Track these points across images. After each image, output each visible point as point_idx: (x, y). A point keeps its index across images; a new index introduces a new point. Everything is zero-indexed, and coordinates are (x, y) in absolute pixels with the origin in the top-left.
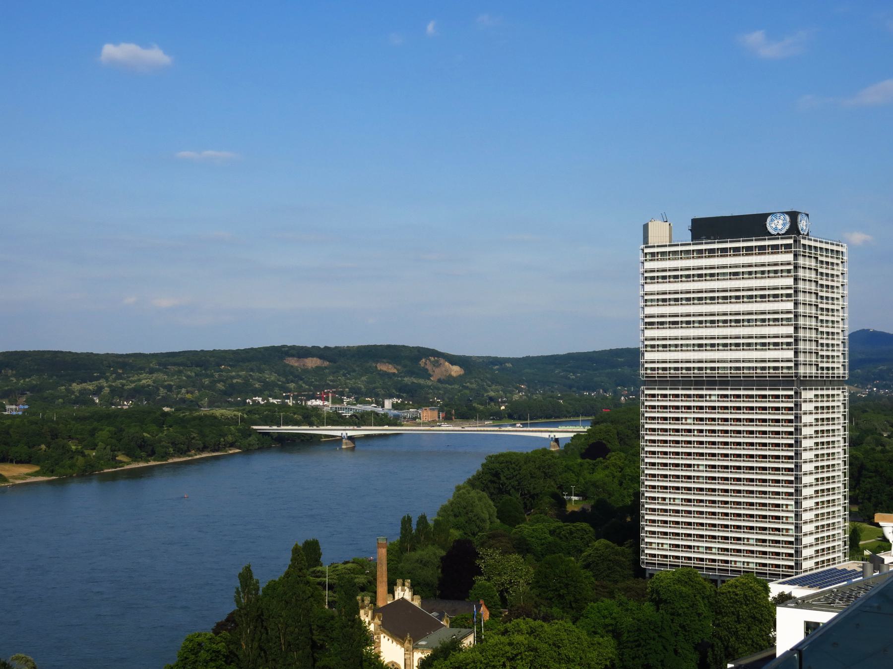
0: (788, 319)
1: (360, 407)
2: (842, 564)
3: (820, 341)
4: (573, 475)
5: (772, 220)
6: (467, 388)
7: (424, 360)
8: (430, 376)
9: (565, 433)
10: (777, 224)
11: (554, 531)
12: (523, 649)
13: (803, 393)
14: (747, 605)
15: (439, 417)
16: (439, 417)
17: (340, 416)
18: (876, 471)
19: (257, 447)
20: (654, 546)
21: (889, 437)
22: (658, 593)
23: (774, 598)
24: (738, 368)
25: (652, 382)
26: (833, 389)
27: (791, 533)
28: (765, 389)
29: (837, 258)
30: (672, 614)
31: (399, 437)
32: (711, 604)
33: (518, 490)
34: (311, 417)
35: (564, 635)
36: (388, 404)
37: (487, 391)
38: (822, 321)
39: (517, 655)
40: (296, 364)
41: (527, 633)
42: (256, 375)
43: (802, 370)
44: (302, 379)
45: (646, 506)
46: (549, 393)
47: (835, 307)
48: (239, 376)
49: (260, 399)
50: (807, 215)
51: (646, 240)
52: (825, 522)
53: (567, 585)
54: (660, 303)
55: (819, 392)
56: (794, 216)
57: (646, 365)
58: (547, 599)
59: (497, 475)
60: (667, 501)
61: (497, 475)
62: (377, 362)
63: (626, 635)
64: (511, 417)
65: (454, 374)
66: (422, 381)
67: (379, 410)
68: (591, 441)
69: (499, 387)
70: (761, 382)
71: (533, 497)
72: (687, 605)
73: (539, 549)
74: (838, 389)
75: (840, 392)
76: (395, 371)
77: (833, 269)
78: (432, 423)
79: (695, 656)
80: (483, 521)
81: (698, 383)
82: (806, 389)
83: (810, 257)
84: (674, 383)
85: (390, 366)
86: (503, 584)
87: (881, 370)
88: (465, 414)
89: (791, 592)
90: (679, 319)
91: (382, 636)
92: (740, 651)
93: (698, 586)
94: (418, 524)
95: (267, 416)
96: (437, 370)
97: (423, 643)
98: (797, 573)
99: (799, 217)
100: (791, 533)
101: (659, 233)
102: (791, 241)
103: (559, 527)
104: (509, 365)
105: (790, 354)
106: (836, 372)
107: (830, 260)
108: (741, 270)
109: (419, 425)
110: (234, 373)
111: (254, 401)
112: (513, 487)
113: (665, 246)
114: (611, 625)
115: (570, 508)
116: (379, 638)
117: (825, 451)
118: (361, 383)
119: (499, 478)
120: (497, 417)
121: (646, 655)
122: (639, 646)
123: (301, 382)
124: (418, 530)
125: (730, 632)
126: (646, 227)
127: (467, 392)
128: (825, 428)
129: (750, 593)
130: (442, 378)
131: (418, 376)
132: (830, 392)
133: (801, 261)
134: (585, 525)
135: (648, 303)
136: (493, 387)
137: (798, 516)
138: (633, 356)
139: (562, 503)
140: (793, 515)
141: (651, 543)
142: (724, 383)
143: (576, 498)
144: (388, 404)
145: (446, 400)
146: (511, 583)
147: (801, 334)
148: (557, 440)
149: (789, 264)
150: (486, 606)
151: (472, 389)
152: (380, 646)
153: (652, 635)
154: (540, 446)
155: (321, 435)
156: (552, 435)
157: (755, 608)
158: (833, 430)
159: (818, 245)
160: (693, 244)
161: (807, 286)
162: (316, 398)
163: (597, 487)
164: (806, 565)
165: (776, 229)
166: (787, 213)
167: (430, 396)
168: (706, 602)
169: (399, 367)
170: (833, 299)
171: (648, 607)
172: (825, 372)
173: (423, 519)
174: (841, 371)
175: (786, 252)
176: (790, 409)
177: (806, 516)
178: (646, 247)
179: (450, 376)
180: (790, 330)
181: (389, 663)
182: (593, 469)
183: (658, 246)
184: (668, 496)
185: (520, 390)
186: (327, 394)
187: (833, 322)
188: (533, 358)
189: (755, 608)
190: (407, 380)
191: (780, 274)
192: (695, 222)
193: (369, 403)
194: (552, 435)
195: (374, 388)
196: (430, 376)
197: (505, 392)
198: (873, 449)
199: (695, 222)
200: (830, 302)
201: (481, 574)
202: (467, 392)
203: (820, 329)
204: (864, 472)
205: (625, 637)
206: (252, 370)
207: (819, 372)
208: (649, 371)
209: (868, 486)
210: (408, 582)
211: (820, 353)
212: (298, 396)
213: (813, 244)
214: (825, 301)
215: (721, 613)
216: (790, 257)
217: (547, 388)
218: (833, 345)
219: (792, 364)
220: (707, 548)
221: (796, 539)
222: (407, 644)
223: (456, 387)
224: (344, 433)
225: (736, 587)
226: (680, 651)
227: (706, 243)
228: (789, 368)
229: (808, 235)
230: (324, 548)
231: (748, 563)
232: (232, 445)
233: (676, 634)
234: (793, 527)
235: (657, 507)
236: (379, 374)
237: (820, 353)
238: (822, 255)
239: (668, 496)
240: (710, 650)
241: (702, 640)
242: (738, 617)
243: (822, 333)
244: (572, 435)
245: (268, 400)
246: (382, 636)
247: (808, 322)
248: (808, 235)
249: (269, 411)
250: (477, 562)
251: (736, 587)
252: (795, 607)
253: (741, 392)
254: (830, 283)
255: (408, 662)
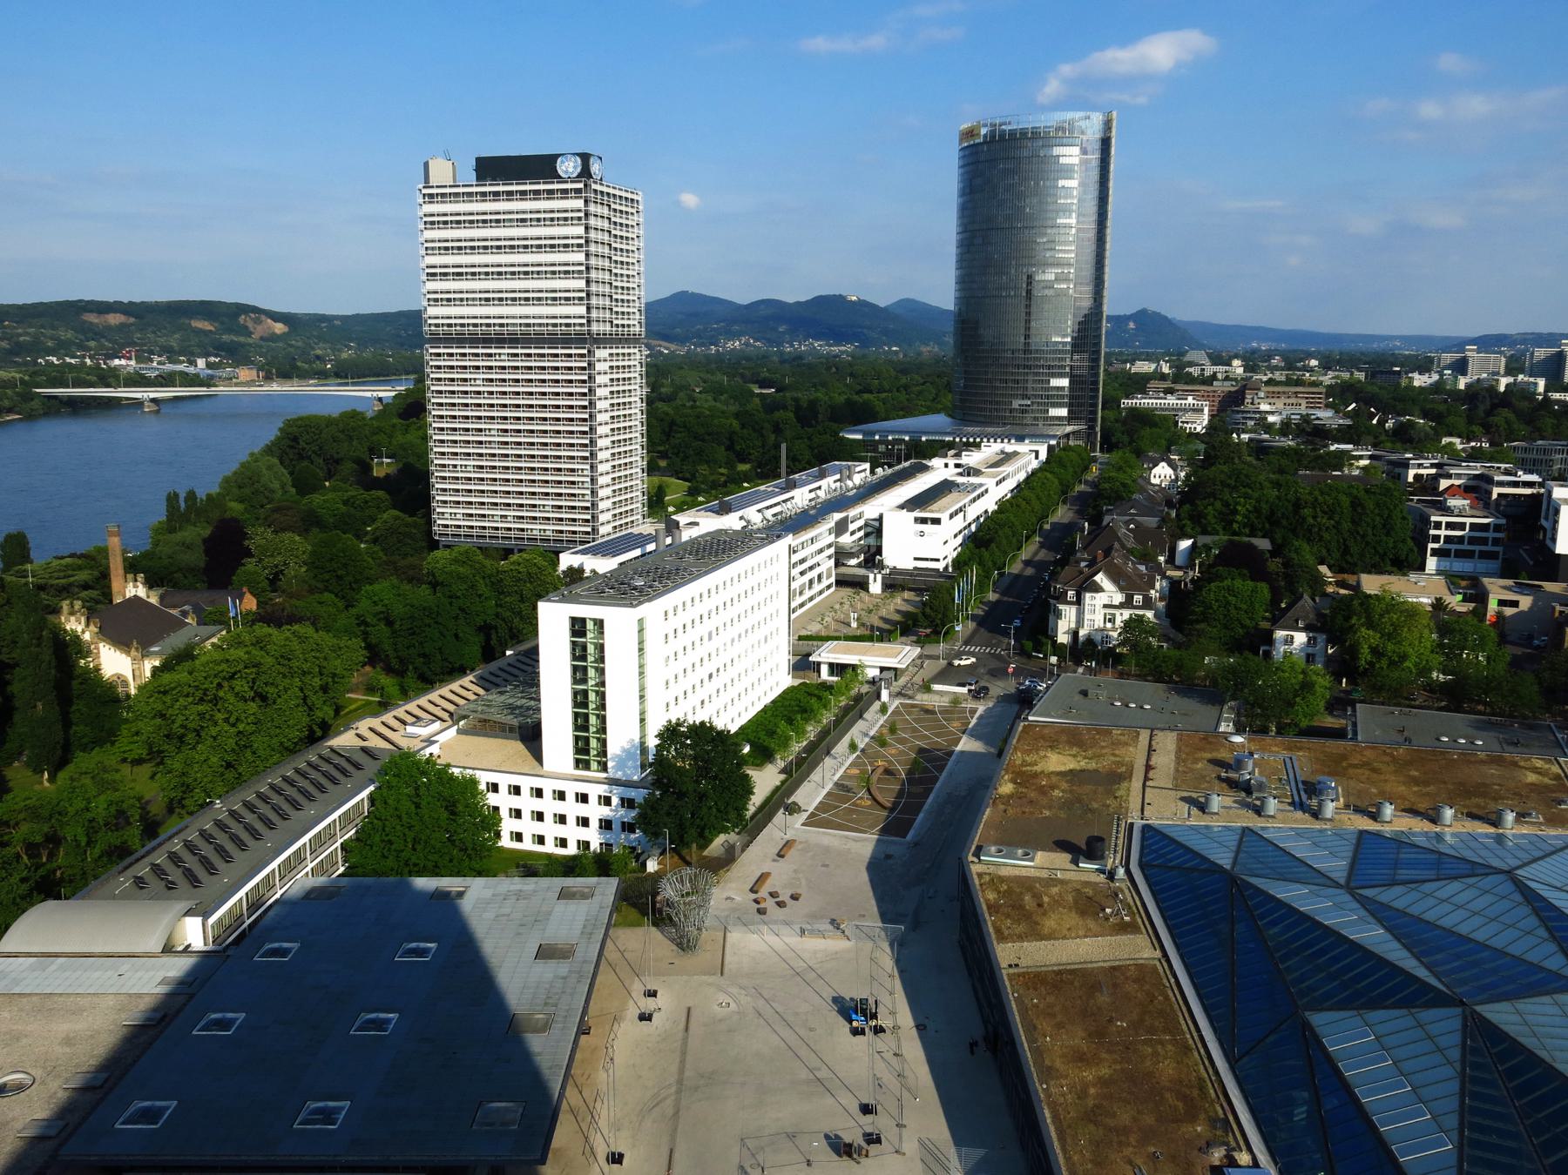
0: (580, 272)
1: (169, 367)
2: (640, 527)
3: (615, 297)
4: (385, 437)
5: (562, 162)
6: (291, 346)
7: (243, 317)
8: (251, 333)
9: (387, 393)
10: (568, 167)
11: (348, 500)
12: (241, 667)
13: (597, 352)
14: (531, 582)
15: (258, 377)
16: (258, 377)
17: (143, 377)
18: (685, 427)
19: (42, 412)
20: (446, 516)
21: (700, 392)
22: (433, 575)
23: (564, 572)
24: (528, 325)
25: (437, 340)
26: (629, 348)
27: (587, 498)
28: (557, 348)
29: (632, 207)
30: (451, 597)
31: (206, 402)
32: (493, 583)
33: (319, 455)
34: (108, 378)
35: (295, 645)
36: (201, 363)
37: (314, 349)
38: (616, 275)
39: (235, 673)
40: (96, 321)
41: (252, 644)
42: (50, 332)
43: (595, 328)
44: (104, 337)
45: (436, 474)
46: (380, 351)
47: (630, 260)
48: (27, 334)
49: (54, 359)
50: (601, 158)
51: (427, 179)
52: (623, 485)
53: (345, 565)
54: (442, 252)
55: (614, 351)
56: (585, 158)
57: (430, 321)
58: (323, 581)
59: (295, 439)
60: (459, 468)
61: (295, 439)
62: (191, 318)
63: (398, 623)
64: (337, 375)
65: (278, 331)
66: (242, 339)
67: (191, 370)
68: (409, 401)
69: (328, 345)
70: (552, 340)
71: (337, 462)
72: (465, 586)
73: (331, 520)
74: (635, 347)
75: (636, 351)
76: (212, 329)
77: (627, 219)
78: (250, 383)
79: (481, 638)
80: (273, 491)
81: (486, 341)
82: (599, 348)
83: (601, 204)
84: (460, 340)
85: (206, 323)
86: (276, 566)
87: (699, 329)
88: (287, 372)
89: (582, 564)
90: (464, 270)
91: (101, 645)
92: (524, 631)
93: (477, 566)
94: (186, 500)
95: (55, 378)
96: (259, 328)
97: (156, 649)
98: (594, 540)
99: (592, 160)
100: (587, 498)
101: (441, 172)
102: (581, 186)
103: (353, 497)
104: (337, 323)
105: (582, 310)
106: (631, 329)
107: (624, 209)
108: (528, 216)
109: (236, 385)
110: (20, 331)
111: (47, 361)
112: (314, 452)
113: (445, 186)
114: (383, 612)
115: (377, 472)
116: (98, 648)
117: (621, 413)
118: (174, 341)
119: (298, 443)
120: (322, 375)
121: (421, 643)
122: (414, 634)
123: (103, 340)
124: (187, 507)
125: (514, 613)
126: (426, 165)
127: (292, 350)
128: (621, 388)
129: (534, 570)
130: (265, 335)
131: (238, 333)
132: (626, 351)
133: (592, 208)
134: (381, 493)
135: (429, 252)
136: (321, 345)
137: (593, 480)
138: (416, 317)
139: (366, 468)
140: (588, 479)
141: (443, 513)
142: (513, 340)
143: (389, 460)
144: (201, 363)
145: (269, 358)
146: (285, 564)
147: (594, 288)
148: (380, 399)
149: (579, 211)
150: (251, 593)
151: (298, 347)
152: (99, 657)
153: (427, 621)
154: (348, 408)
155: (121, 398)
156: (375, 394)
157: (539, 585)
158: (630, 391)
159: (611, 191)
160: (476, 185)
161: (600, 236)
162: (120, 358)
163: (405, 450)
164: (603, 530)
165: (566, 172)
166: (578, 154)
167: (251, 354)
168: (487, 581)
169: (216, 325)
170: (627, 251)
171: (425, 590)
172: (620, 329)
173: (191, 495)
174: (637, 329)
175: (576, 198)
176: (584, 369)
177: (602, 480)
178: (424, 187)
179: (274, 334)
180: (582, 284)
181: (113, 676)
182: (406, 430)
183: (437, 187)
184: (459, 463)
185: (350, 348)
186: (129, 352)
187: (628, 276)
188: (363, 315)
189: (539, 585)
190: (225, 338)
191: (570, 222)
192: (480, 161)
193: (182, 362)
194: (375, 394)
195: (189, 346)
196: (251, 333)
197: (333, 350)
198: (684, 405)
199: (480, 161)
200: (625, 254)
201: (251, 556)
202: (292, 350)
203: (614, 284)
204: (675, 428)
205: (397, 626)
206: (43, 327)
207: (614, 329)
208: (433, 328)
209: (677, 441)
210: (141, 576)
211: (615, 309)
212: (95, 354)
213: (605, 189)
214: (619, 253)
215: (503, 593)
216: (580, 204)
217: (378, 346)
218: (628, 301)
219: (584, 321)
220: (502, 516)
221: (593, 505)
222: (133, 652)
223: (281, 344)
224: (145, 395)
225: (519, 564)
226: (461, 635)
227: (490, 185)
228: (581, 325)
229: (601, 180)
230: (33, 540)
231: (545, 530)
232: (10, 411)
233: (456, 618)
234: (589, 492)
235: (447, 475)
236: (194, 331)
237: (615, 309)
238: (615, 203)
239: (459, 463)
240: (493, 631)
241: (485, 622)
242: (521, 596)
243: (616, 287)
244: (393, 394)
245: (64, 360)
246: (101, 645)
247: (601, 276)
248: (601, 180)
249: (58, 371)
250: (246, 543)
251: (519, 564)
252: (559, 601)
253: (532, 351)
254: (624, 234)
255: (137, 673)
